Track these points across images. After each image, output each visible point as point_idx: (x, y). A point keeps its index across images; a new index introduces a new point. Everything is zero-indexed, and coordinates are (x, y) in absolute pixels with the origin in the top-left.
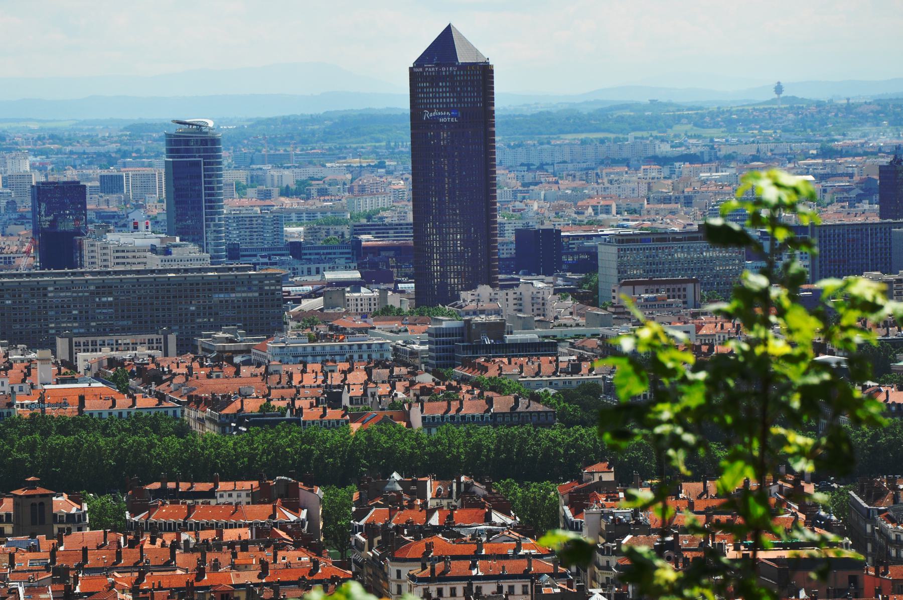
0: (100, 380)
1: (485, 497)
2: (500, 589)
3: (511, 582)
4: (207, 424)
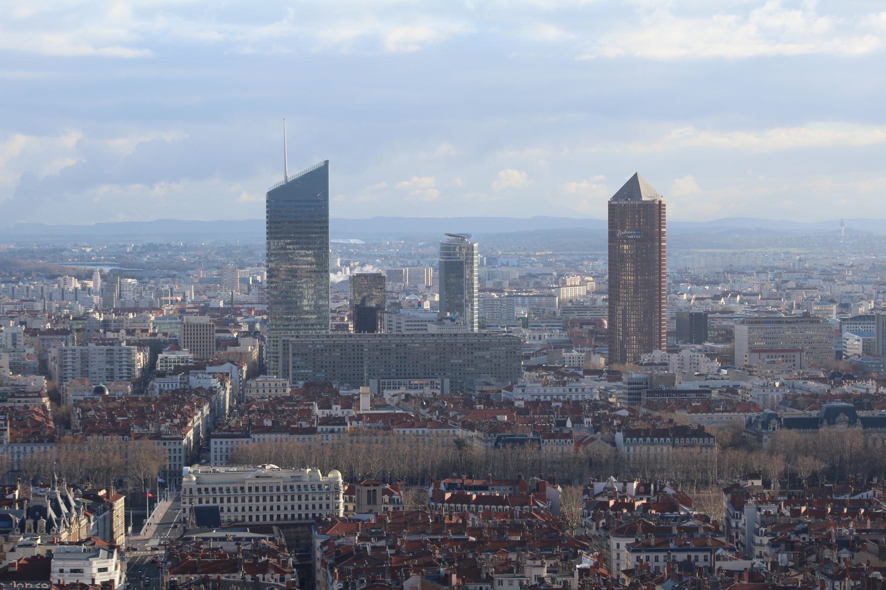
0: (401, 408)
1: (674, 495)
2: (689, 557)
3: (697, 554)
4: (475, 440)
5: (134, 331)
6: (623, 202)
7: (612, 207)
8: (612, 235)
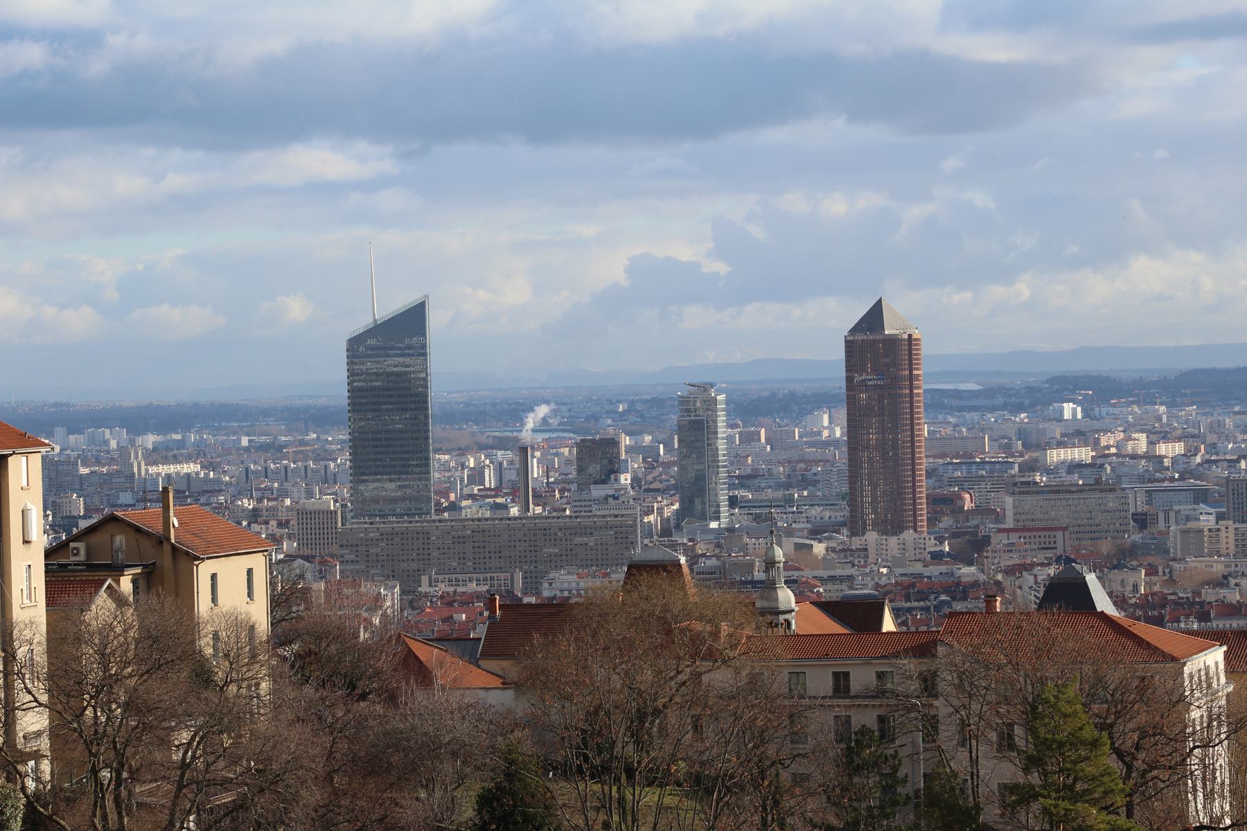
5: (288, 522)
6: (860, 337)
7: (850, 345)
8: (849, 380)
